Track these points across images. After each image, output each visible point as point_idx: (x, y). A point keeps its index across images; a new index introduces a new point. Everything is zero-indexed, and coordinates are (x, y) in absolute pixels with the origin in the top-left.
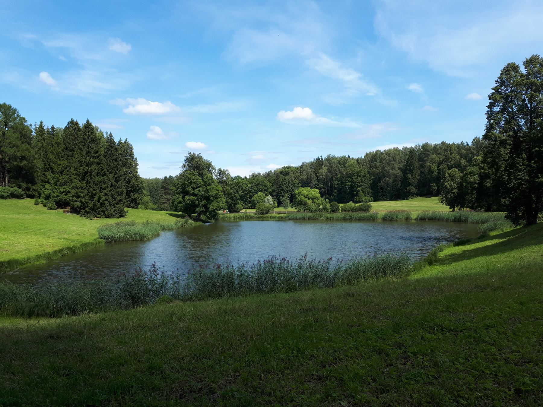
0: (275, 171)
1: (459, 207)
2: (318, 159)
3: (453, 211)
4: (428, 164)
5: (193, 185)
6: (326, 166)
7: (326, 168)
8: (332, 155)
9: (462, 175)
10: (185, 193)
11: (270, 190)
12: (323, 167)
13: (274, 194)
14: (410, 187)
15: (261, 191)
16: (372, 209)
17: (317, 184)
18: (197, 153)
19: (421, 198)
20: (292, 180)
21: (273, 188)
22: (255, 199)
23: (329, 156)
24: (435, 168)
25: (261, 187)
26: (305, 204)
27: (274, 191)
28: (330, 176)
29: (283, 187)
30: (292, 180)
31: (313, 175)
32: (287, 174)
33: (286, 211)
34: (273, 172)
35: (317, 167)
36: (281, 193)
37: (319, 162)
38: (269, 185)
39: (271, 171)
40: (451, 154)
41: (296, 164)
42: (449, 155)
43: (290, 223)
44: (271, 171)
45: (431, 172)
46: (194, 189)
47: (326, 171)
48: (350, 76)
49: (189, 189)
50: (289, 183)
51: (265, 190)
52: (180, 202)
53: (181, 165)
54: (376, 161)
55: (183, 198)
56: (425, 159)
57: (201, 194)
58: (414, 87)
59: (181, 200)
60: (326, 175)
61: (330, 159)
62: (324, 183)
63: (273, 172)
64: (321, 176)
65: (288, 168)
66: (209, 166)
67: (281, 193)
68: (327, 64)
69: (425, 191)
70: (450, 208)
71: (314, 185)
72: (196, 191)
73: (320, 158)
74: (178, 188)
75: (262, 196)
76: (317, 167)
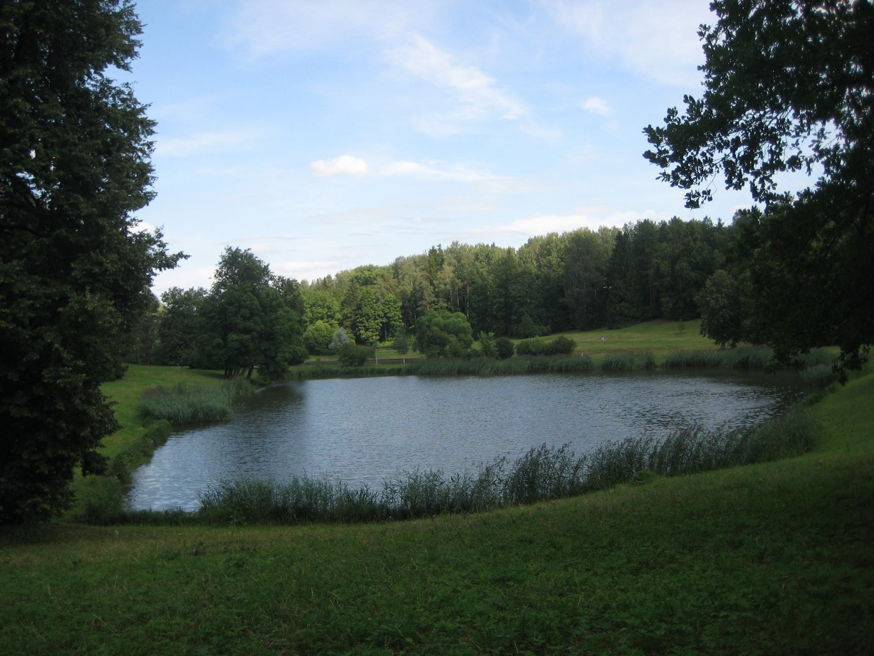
0: (337, 276)
1: (731, 341)
2: (433, 251)
3: (723, 349)
4: (655, 260)
5: (245, 312)
6: (449, 264)
7: (452, 268)
8: (462, 242)
9: (736, 283)
10: (228, 328)
11: (338, 316)
12: (445, 266)
13: (348, 323)
14: (623, 304)
15: (322, 318)
16: (577, 349)
17: (434, 302)
18: (243, 249)
19: (645, 324)
20: (382, 295)
21: (345, 311)
22: (310, 334)
23: (455, 244)
24: (665, 267)
25: (320, 310)
26: (443, 343)
27: (346, 317)
28: (460, 284)
29: (366, 310)
30: (382, 295)
31: (425, 283)
32: (367, 282)
33: (403, 357)
34: (333, 277)
35: (431, 266)
36: (361, 322)
37: (435, 259)
38: (336, 306)
39: (329, 277)
40: (695, 241)
41: (383, 260)
42: (691, 243)
43: (412, 380)
44: (329, 277)
45: (659, 275)
46: (244, 318)
47: (452, 275)
48: (471, 82)
49: (238, 320)
50: (378, 300)
51: (329, 316)
52: (218, 346)
53: (212, 273)
54: (549, 254)
55: (224, 337)
56: (647, 250)
57: (258, 328)
58: (594, 104)
59: (220, 341)
60: (453, 284)
61: (457, 252)
62: (448, 300)
63: (333, 277)
64: (442, 286)
65: (370, 269)
66: (265, 271)
67: (361, 322)
68: (427, 58)
69: (684, 311)
70: (716, 343)
71: (430, 304)
72: (250, 324)
73: (436, 248)
74: (213, 318)
75: (324, 328)
76: (431, 266)
